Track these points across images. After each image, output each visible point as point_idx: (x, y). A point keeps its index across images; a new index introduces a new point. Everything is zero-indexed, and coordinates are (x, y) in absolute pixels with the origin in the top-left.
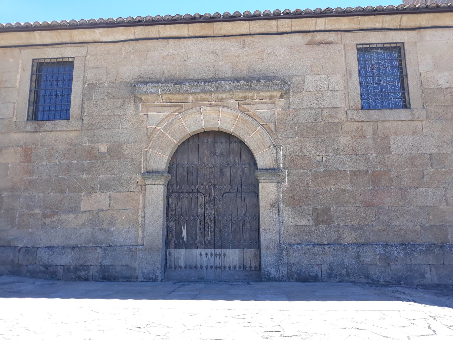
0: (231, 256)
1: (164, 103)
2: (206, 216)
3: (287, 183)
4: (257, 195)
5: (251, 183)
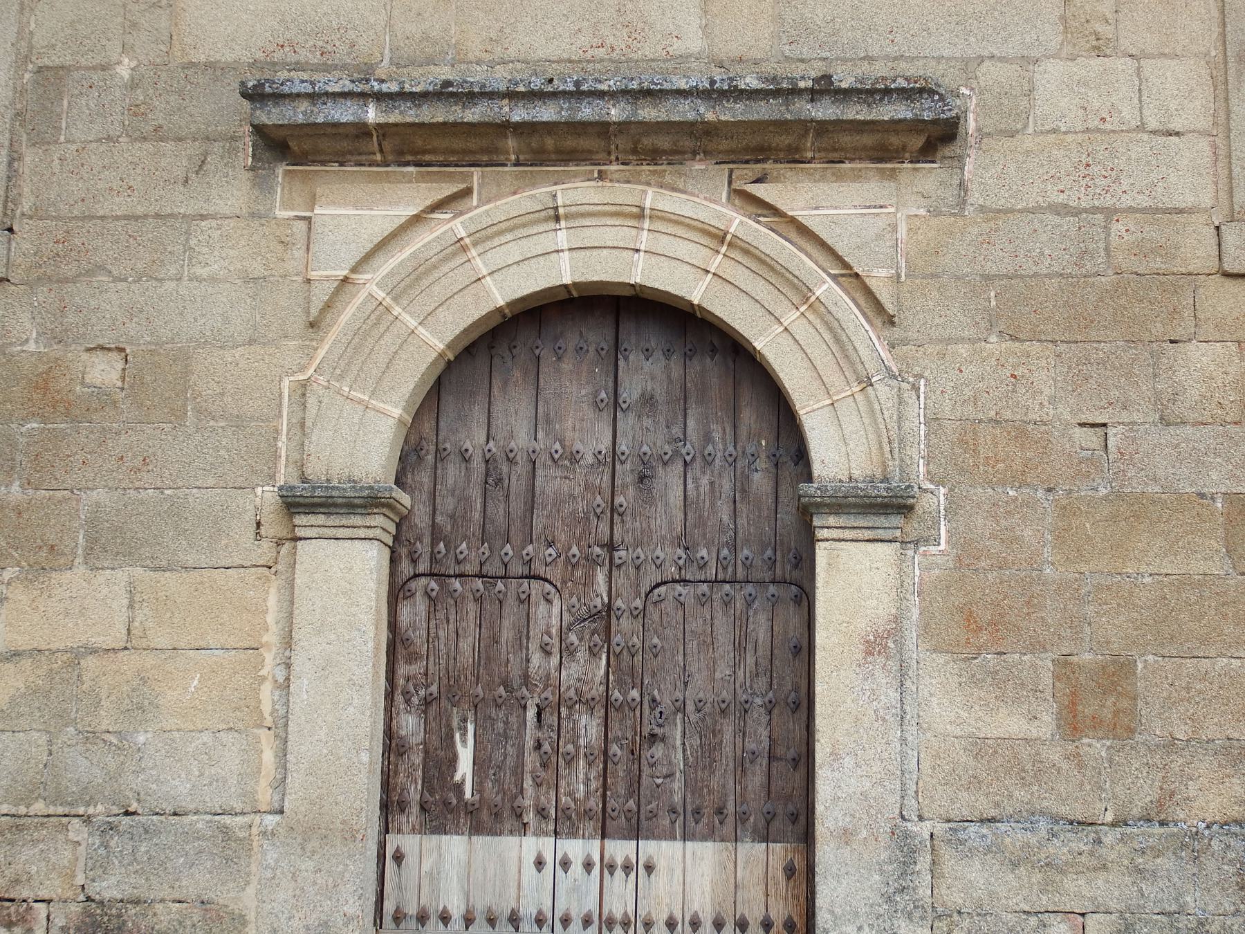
0: (679, 872)
1: (388, 166)
2: (568, 689)
3: (942, 547)
4: (805, 598)
5: (782, 544)
